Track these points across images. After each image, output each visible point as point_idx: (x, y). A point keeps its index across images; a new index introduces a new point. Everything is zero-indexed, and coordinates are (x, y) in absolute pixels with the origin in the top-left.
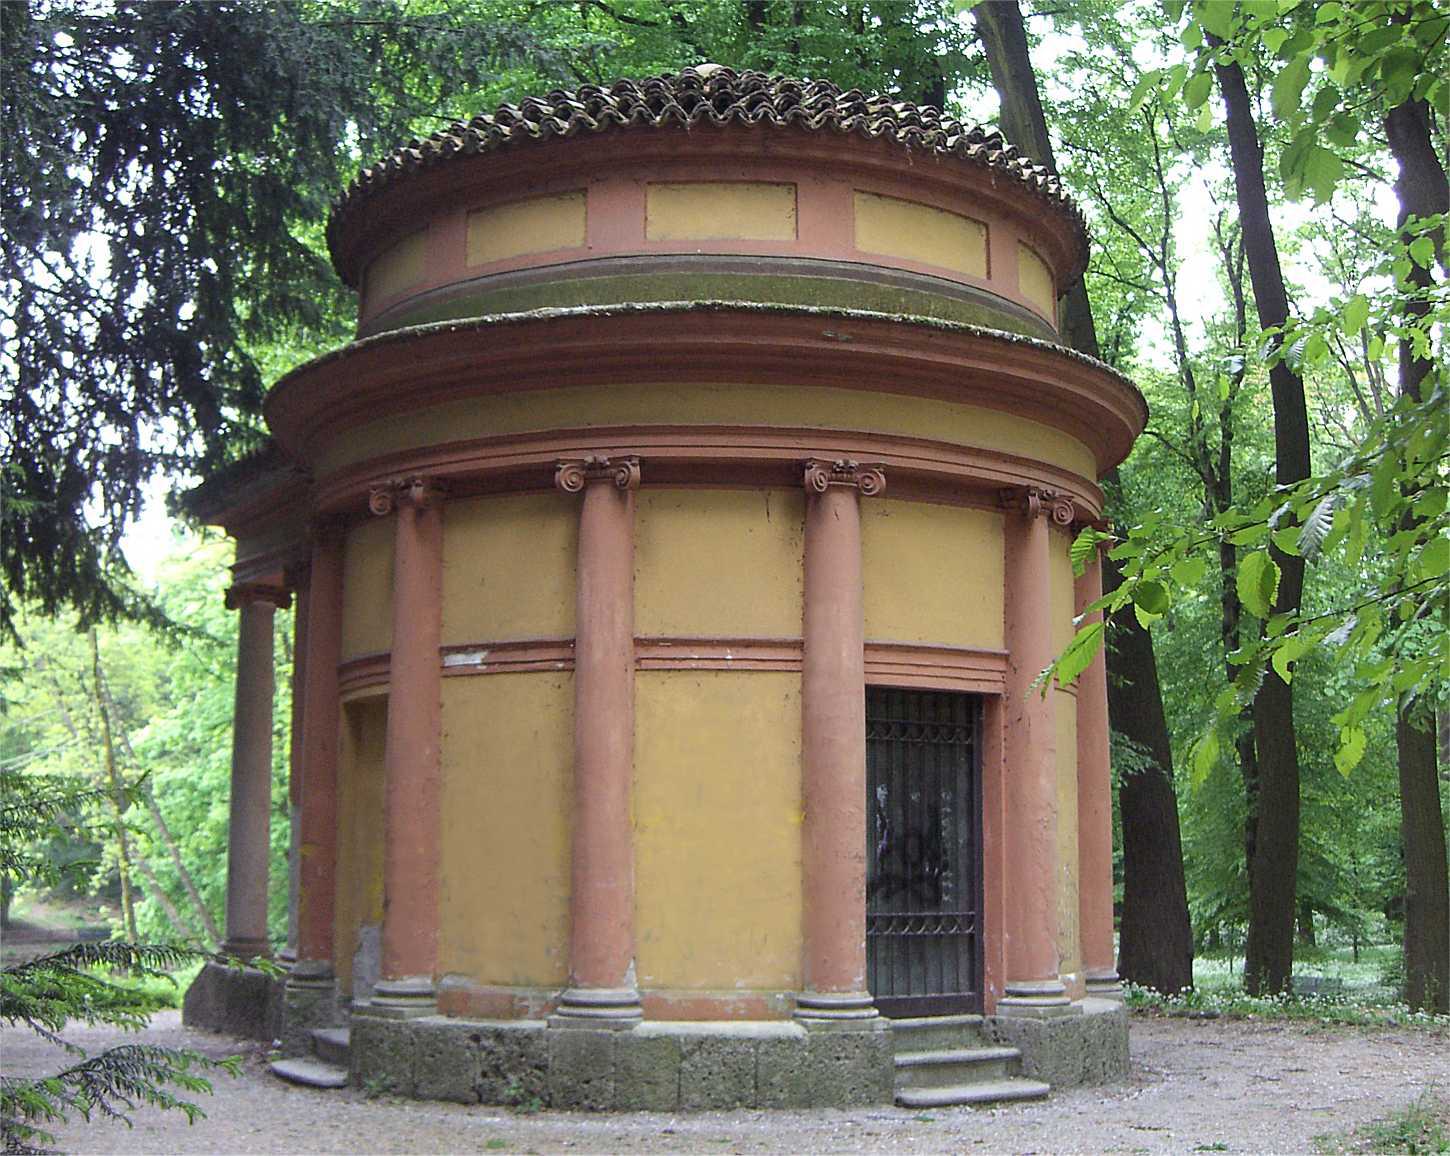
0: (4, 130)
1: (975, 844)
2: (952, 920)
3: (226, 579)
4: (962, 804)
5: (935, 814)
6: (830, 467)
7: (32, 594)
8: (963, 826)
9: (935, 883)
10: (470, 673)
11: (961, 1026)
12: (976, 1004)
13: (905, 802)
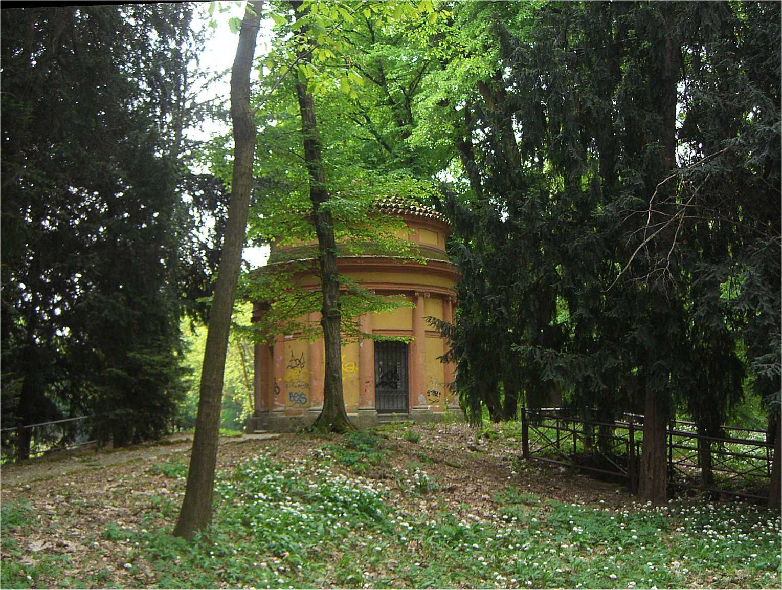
0: (9, 151)
1: (406, 375)
2: (401, 392)
3: (251, 315)
4: (403, 365)
5: (396, 368)
6: (419, 292)
7: (200, 321)
8: (403, 370)
9: (396, 383)
10: (290, 340)
11: (402, 416)
12: (407, 411)
13: (388, 365)
